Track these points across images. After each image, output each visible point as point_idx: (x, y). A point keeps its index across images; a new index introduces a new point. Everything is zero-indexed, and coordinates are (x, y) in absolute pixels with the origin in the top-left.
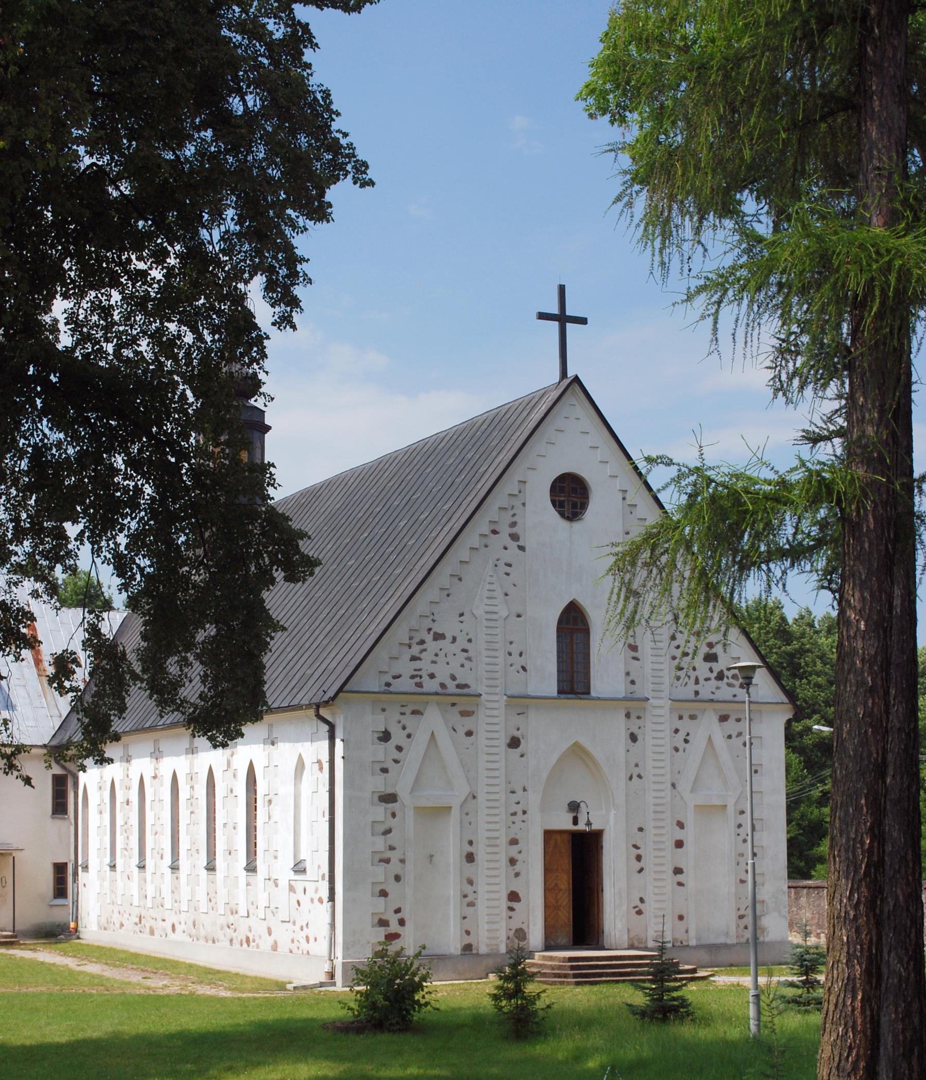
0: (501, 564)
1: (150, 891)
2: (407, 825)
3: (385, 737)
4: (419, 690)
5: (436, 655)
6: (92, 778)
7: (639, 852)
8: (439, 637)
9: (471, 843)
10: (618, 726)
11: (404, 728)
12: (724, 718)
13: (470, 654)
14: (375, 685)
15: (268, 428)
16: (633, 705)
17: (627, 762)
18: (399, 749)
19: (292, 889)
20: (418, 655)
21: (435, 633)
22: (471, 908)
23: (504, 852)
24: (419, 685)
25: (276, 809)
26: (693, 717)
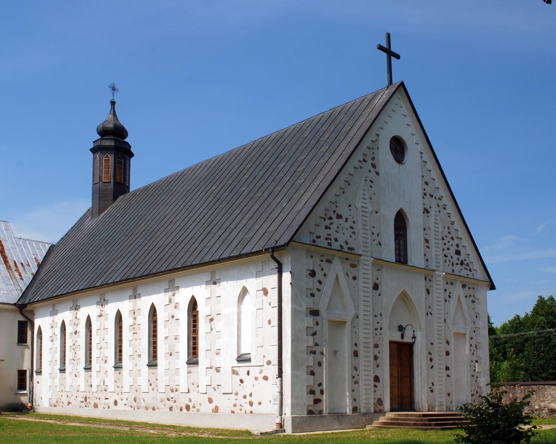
0: (368, 180)
1: (95, 382)
2: (325, 330)
3: (313, 274)
4: (330, 247)
5: (338, 228)
6: (45, 322)
7: (432, 356)
8: (339, 217)
9: (356, 345)
10: (421, 284)
11: (322, 270)
12: (464, 286)
13: (355, 230)
14: (307, 239)
15: (132, 155)
16: (428, 274)
17: (426, 305)
18: (320, 282)
19: (234, 372)
20: (329, 226)
21: (337, 214)
22: (356, 385)
23: (372, 352)
24: (330, 244)
25: (218, 325)
26: (452, 284)
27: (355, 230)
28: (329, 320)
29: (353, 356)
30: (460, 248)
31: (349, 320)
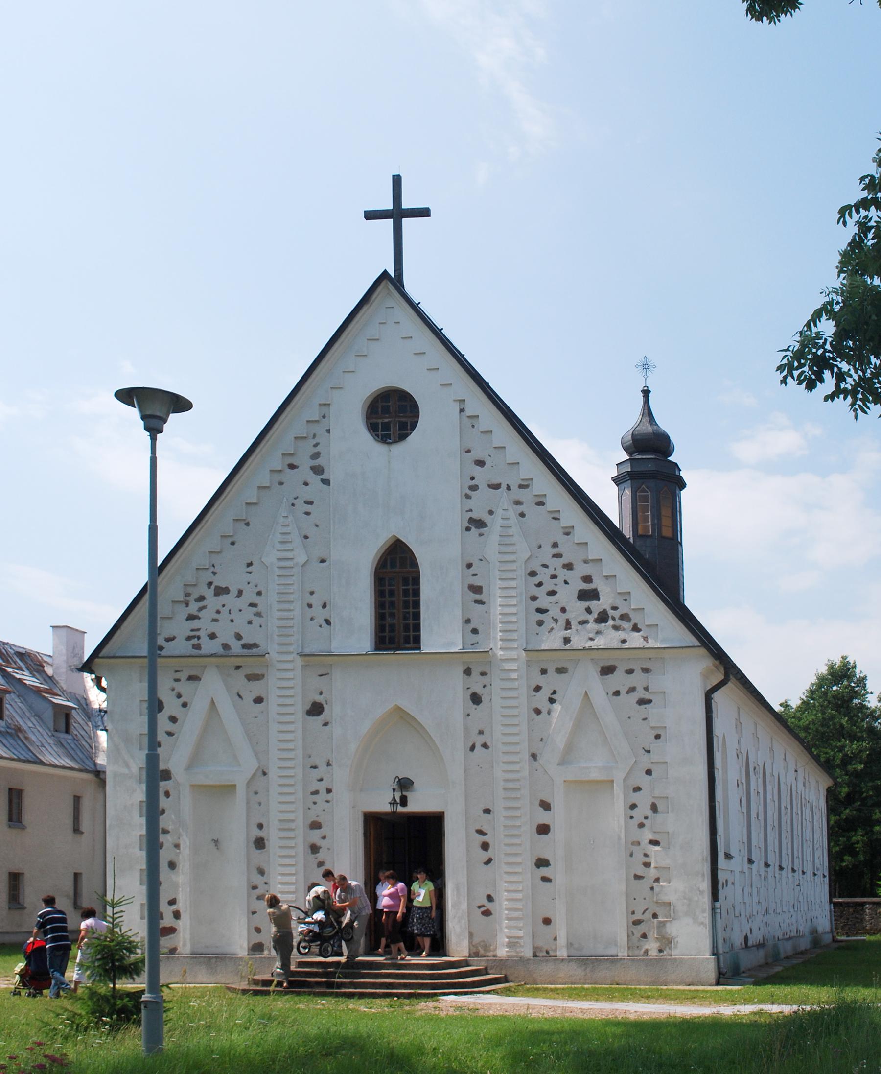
7: (485, 838)
8: (221, 591)
13: (260, 608)
20: (196, 613)
26: (561, 671)
27: (260, 608)
28: (192, 786)
29: (265, 839)
30: (598, 584)
31: (241, 783)
